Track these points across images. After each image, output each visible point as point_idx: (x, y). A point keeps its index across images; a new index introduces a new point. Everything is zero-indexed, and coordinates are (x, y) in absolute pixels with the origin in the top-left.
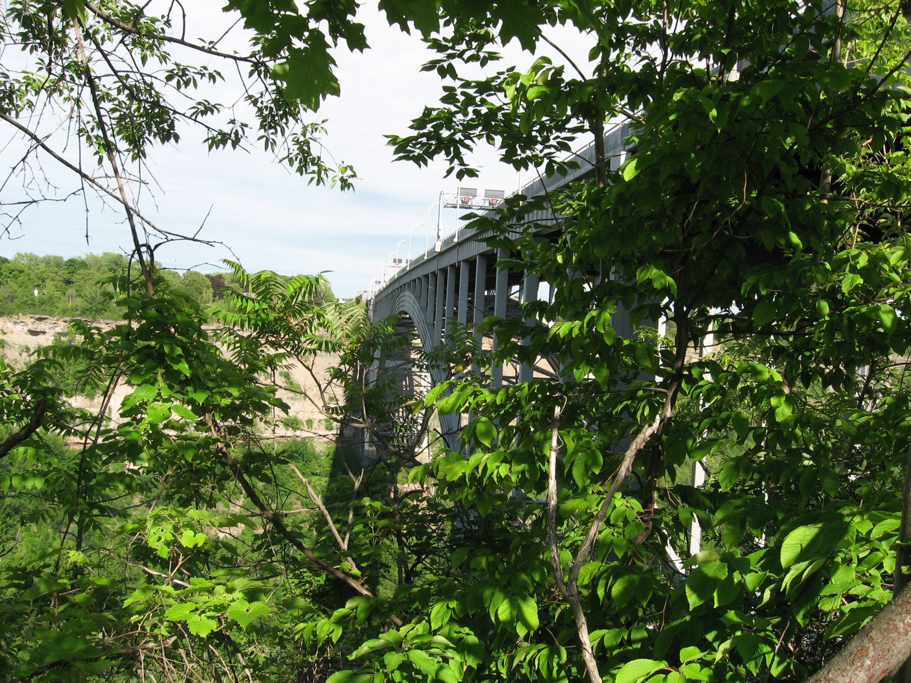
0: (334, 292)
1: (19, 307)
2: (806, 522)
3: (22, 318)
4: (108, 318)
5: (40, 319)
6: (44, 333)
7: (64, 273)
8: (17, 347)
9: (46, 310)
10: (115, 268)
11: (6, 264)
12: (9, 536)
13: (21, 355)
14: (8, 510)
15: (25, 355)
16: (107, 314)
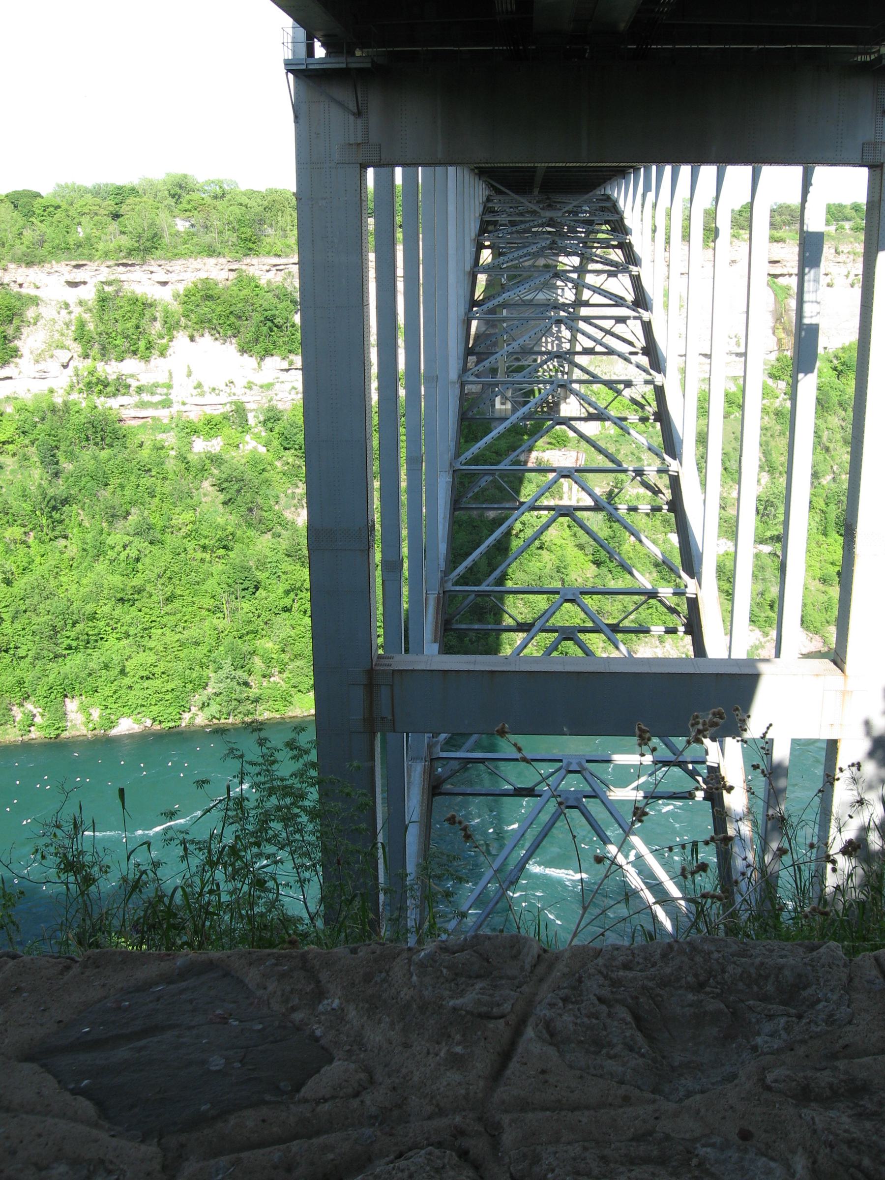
0: (261, 187)
1: (50, 253)
2: (673, 925)
3: (56, 266)
4: (160, 258)
5: (78, 266)
6: (85, 283)
7: (110, 204)
8: (53, 303)
9: (84, 255)
10: (179, 191)
11: (39, 200)
12: (57, 533)
13: (59, 313)
14: (53, 502)
15: (64, 312)
16: (158, 253)
